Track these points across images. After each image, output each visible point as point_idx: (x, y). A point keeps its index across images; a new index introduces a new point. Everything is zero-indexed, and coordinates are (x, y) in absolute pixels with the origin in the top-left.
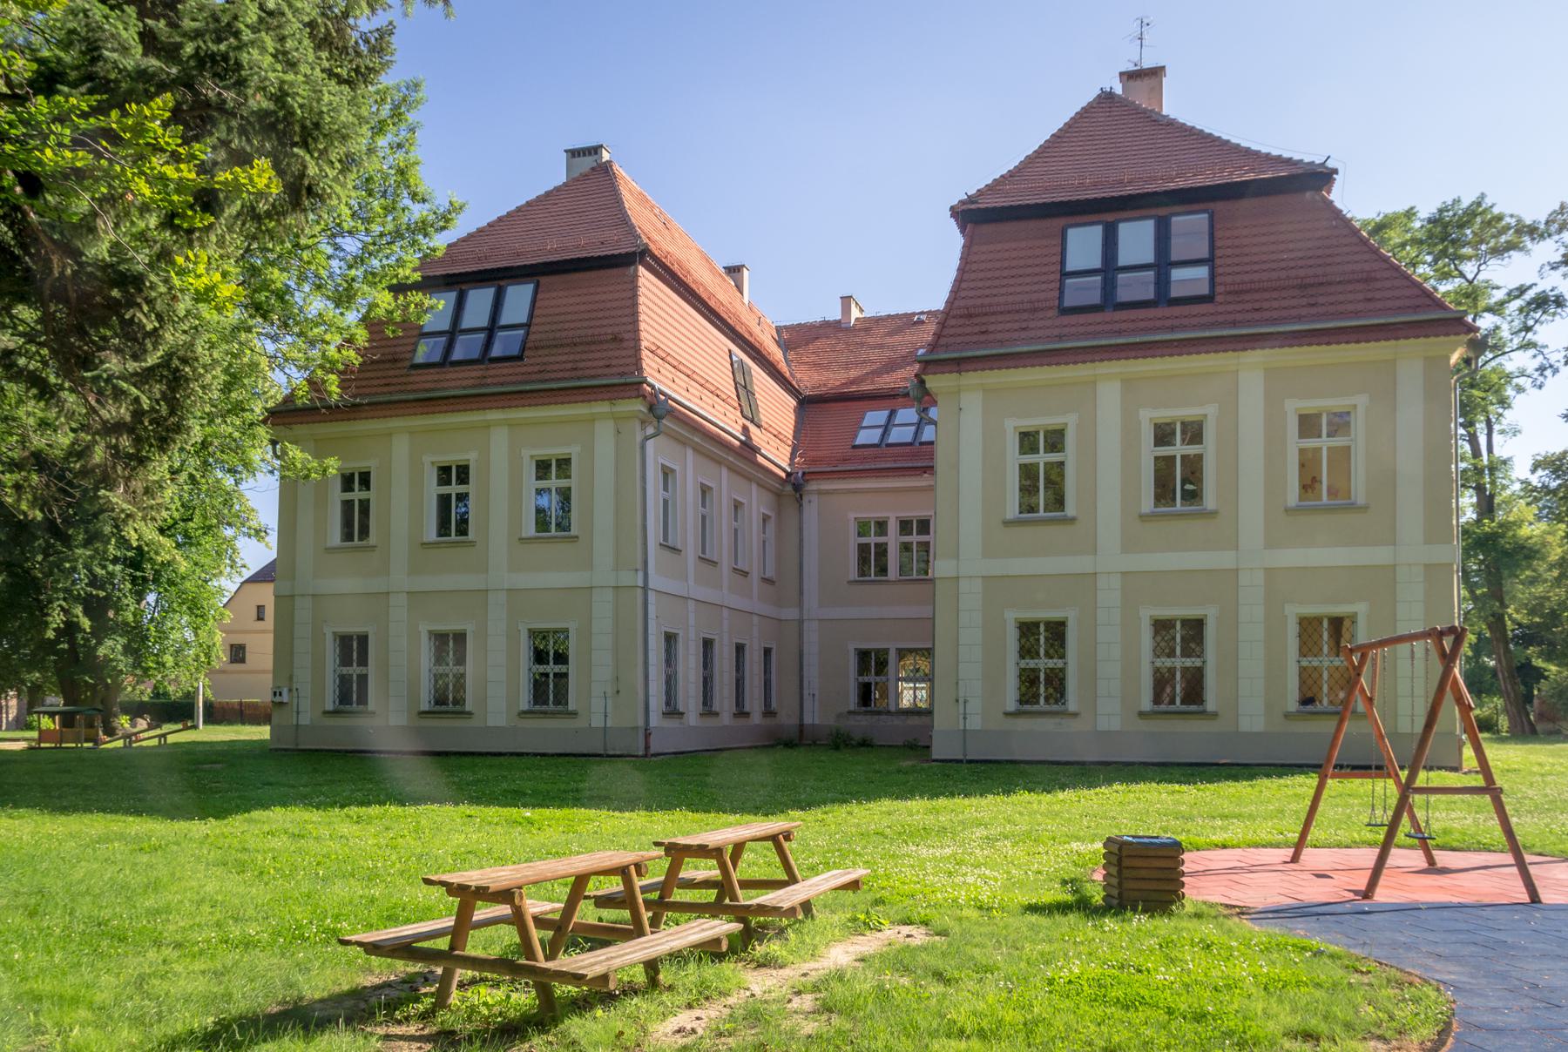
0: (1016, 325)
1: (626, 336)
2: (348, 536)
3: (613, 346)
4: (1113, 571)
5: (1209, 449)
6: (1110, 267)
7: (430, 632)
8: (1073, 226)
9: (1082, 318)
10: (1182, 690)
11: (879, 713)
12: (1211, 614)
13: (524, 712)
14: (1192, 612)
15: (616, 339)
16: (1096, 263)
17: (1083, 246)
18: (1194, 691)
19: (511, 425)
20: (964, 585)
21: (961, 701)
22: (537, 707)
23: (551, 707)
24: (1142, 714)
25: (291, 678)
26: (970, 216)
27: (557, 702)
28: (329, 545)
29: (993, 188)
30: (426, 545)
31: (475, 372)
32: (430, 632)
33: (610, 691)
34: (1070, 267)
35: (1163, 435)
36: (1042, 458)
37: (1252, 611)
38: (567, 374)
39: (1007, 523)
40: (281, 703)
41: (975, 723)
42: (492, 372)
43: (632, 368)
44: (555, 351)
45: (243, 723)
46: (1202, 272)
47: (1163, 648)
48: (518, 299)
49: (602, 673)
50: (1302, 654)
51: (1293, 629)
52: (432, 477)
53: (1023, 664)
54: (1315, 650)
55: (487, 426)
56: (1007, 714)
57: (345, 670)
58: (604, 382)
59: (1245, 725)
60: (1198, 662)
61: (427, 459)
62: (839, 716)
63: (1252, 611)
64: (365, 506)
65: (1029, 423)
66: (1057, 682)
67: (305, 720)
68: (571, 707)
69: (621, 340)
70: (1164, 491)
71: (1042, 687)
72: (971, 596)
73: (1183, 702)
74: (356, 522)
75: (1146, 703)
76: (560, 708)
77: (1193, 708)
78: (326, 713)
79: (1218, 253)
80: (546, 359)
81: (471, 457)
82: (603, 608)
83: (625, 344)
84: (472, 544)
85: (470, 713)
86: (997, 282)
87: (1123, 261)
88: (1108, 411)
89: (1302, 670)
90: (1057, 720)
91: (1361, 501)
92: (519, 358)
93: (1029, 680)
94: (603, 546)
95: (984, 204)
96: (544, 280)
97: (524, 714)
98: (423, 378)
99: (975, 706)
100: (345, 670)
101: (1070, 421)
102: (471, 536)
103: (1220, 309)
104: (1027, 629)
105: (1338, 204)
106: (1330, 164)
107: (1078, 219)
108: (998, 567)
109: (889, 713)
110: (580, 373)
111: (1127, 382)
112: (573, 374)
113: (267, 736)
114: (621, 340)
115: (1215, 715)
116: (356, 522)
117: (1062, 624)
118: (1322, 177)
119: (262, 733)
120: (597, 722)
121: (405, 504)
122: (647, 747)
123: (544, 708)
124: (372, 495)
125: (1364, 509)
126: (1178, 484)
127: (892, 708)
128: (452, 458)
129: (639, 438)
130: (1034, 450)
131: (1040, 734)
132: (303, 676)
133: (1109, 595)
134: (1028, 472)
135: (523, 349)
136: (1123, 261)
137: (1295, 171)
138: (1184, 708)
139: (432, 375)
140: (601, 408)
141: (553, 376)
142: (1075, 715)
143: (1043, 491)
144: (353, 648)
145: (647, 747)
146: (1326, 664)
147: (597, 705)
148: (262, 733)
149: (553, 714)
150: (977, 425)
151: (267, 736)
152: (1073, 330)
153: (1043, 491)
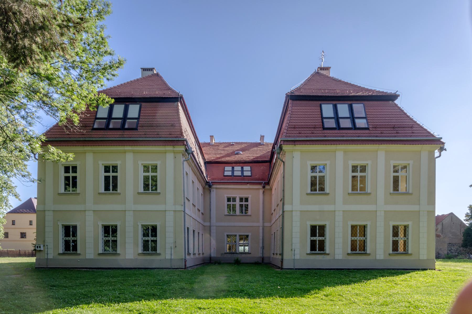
0: (310, 132)
1: (176, 125)
2: (107, 188)
3: (172, 128)
4: (339, 211)
5: (159, 174)
6: (125, 118)
7: (102, 225)
8: (324, 104)
9: (331, 131)
11: (234, 253)
12: (369, 223)
13: (140, 254)
15: (173, 125)
16: (121, 116)
17: (328, 110)
18: (363, 247)
19: (134, 152)
20: (337, 213)
21: (293, 250)
22: (145, 252)
23: (317, 251)
24: (348, 254)
25: (44, 241)
26: (294, 98)
27: (73, 250)
28: (100, 192)
29: (298, 89)
30: (139, 193)
31: (120, 133)
32: (102, 225)
33: (172, 246)
34: (98, 116)
35: (354, 169)
36: (111, 174)
37: (380, 224)
38: (156, 136)
40: (40, 251)
41: (297, 257)
42: (126, 133)
43: (180, 136)
44: (149, 128)
45: (9, 257)
46: (364, 121)
47: (354, 233)
48: (134, 110)
49: (170, 240)
50: (352, 236)
52: (141, 169)
53: (144, 238)
54: (356, 235)
55: (125, 152)
56: (307, 254)
57: (67, 239)
58: (381, 139)
59: (378, 257)
60: (323, 238)
61: (100, 163)
62: (222, 254)
63: (380, 224)
64: (115, 178)
65: (356, 163)
66: (322, 244)
67: (50, 257)
69: (175, 126)
70: (146, 186)
71: (358, 247)
72: (296, 217)
73: (319, 250)
74: (71, 183)
76: (74, 252)
77: (322, 252)
78: (59, 254)
79: (141, 117)
80: (147, 130)
81: (118, 163)
82: (170, 217)
83: (176, 128)
84: (119, 194)
85: (119, 254)
86: (299, 119)
87: (114, 116)
88: (338, 160)
89: (352, 241)
90: (323, 256)
91: (410, 192)
92: (136, 129)
94: (170, 196)
95: (297, 94)
96: (143, 104)
97: (139, 254)
98: (109, 133)
99: (297, 252)
100: (67, 239)
101: (158, 163)
102: (119, 190)
103: (371, 132)
105: (399, 105)
106: (397, 93)
107: (356, 102)
108: (305, 208)
109: (237, 253)
110: (383, 135)
111: (345, 152)
112: (158, 136)
113: (34, 261)
114: (175, 126)
115: (369, 254)
116: (71, 183)
118: (393, 97)
119: (33, 260)
120: (168, 257)
121: (379, 180)
122: (185, 265)
123: (148, 252)
124: (78, 175)
125: (411, 194)
126: (111, 184)
127: (238, 252)
128: (110, 163)
129: (182, 160)
130: (108, 171)
131: (399, 260)
132: (49, 240)
133: (339, 218)
134: (107, 178)
135: (137, 126)
136: (114, 116)
137: (384, 94)
138: (319, 252)
139: (102, 132)
140: (169, 148)
141: (385, 135)
142: (328, 254)
143: (317, 186)
144: (70, 231)
145: (185, 265)
146: (359, 239)
147: (168, 251)
148: (33, 260)
150: (297, 164)
151: (34, 261)
152: (331, 135)
153: (317, 186)
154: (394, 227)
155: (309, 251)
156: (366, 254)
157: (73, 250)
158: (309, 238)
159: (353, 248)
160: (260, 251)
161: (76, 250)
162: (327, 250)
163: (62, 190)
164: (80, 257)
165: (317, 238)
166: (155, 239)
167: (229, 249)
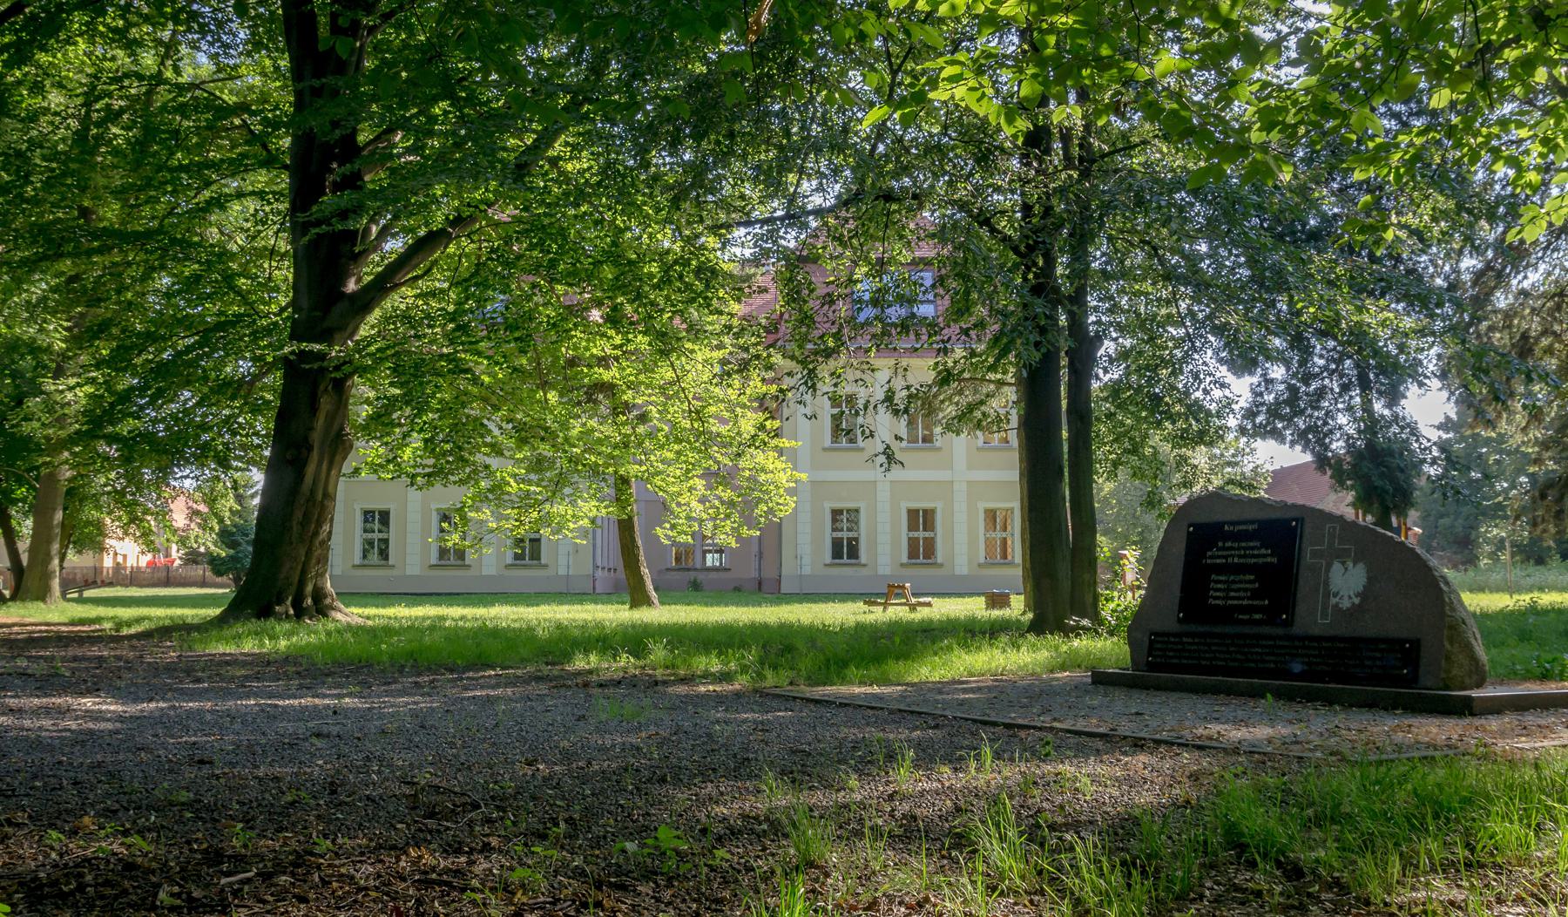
10: (846, 550)
12: (939, 506)
14: (383, 507)
18: (854, 553)
20: (956, 487)
23: (845, 560)
27: (532, 558)
39: (825, 449)
41: (807, 570)
47: (913, 526)
51: (982, 516)
59: (958, 571)
68: (543, 561)
75: (905, 559)
89: (987, 539)
93: (913, 545)
97: (508, 566)
99: (806, 560)
104: (913, 514)
115: (941, 565)
117: (933, 511)
120: (562, 571)
147: (562, 561)
149: (530, 566)
154: (987, 511)
155: (828, 559)
156: (934, 564)
157: (532, 558)
158: (904, 534)
159: (913, 554)
160: (754, 564)
161: (857, 557)
162: (863, 558)
163: (828, 442)
164: (395, 572)
165: (921, 534)
166: (835, 534)
167: (678, 559)
